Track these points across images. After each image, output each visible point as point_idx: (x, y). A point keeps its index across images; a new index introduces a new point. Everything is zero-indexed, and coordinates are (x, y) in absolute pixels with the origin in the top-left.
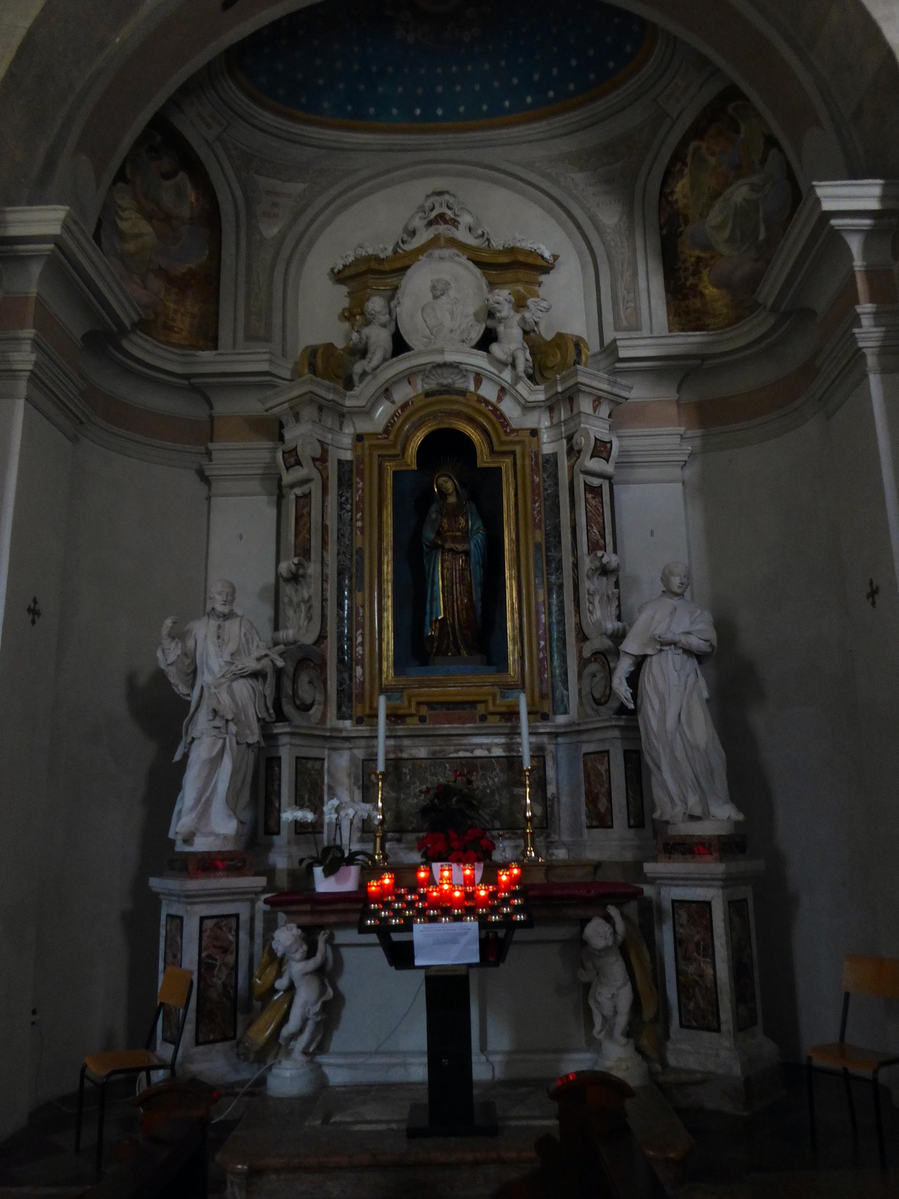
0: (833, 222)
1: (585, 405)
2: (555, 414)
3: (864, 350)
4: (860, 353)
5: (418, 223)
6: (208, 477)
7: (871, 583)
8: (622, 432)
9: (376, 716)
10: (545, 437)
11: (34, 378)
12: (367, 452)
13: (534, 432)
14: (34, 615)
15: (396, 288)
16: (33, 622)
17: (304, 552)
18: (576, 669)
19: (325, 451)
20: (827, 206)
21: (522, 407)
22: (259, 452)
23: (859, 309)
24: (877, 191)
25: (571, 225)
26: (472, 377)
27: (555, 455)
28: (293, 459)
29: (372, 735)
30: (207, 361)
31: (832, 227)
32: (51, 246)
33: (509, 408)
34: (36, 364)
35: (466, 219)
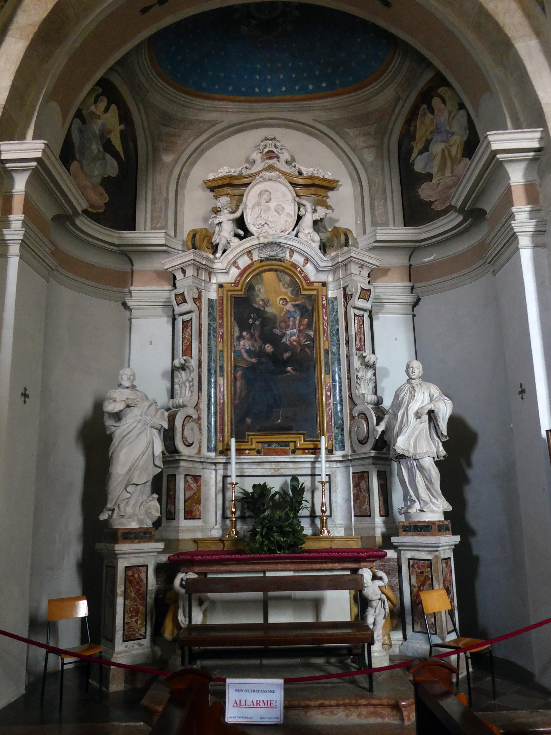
0: (498, 156)
1: (354, 269)
2: (336, 275)
3: (517, 234)
4: (515, 235)
5: (257, 156)
6: (129, 307)
7: (521, 386)
8: (374, 284)
9: (230, 449)
10: (330, 286)
11: (24, 244)
12: (225, 293)
13: (324, 285)
14: (25, 397)
15: (242, 195)
16: (25, 402)
17: (187, 351)
18: (350, 567)
19: (200, 293)
20: (495, 146)
21: (315, 267)
22: (162, 292)
25: (345, 158)
26: (288, 251)
27: (335, 298)
28: (181, 299)
29: (228, 461)
30: (129, 236)
31: (498, 159)
32: (35, 164)
33: (309, 269)
35: (285, 156)
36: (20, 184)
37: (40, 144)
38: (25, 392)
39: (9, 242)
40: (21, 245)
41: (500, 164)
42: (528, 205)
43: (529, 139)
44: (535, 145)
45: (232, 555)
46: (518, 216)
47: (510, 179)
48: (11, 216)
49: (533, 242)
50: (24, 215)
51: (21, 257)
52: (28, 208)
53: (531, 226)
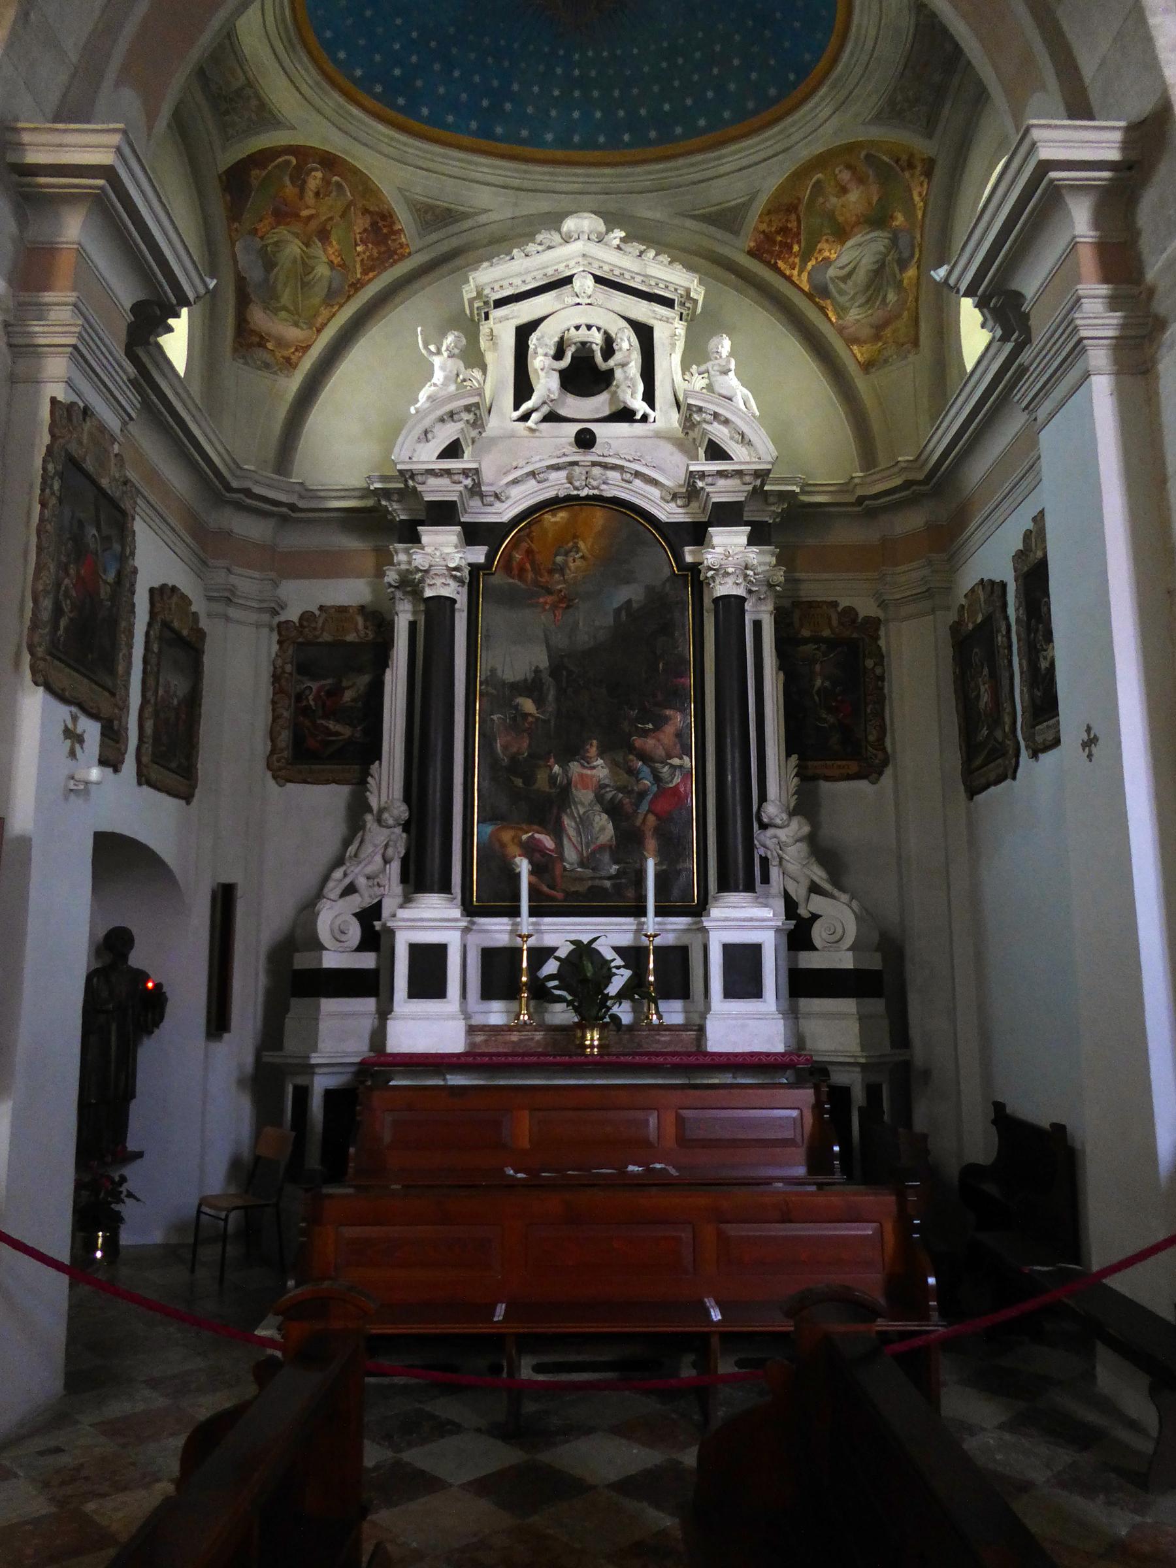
0: (1053, 175)
31: (1052, 181)
44: (1114, 155)
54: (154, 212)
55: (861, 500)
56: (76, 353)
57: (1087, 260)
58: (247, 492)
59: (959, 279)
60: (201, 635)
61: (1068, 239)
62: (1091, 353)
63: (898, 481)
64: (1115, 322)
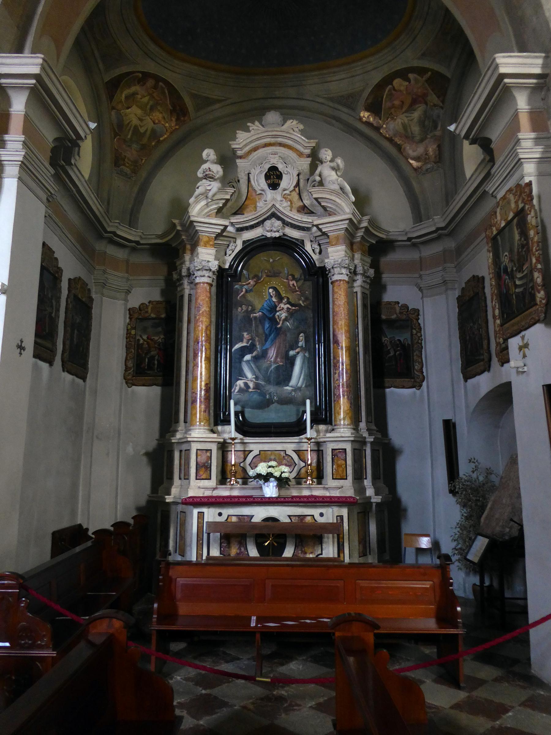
0: (506, 80)
11: (24, 166)
14: (21, 349)
23: (521, 136)
24: (540, 61)
31: (505, 84)
32: (34, 81)
34: (25, 157)
36: (18, 105)
37: (38, 59)
38: (21, 351)
39: (5, 162)
40: (21, 166)
41: (507, 89)
42: (534, 132)
43: (531, 64)
44: (537, 71)
45: (63, 166)
46: (524, 144)
47: (517, 105)
48: (6, 136)
49: (538, 169)
50: (24, 136)
51: (20, 179)
52: (29, 129)
53: (537, 152)
54: (65, 101)
55: (409, 239)
56: (23, 165)
57: (524, 120)
58: (114, 233)
59: (461, 130)
60: (91, 300)
61: (514, 111)
62: (525, 165)
63: (433, 229)
64: (540, 150)
